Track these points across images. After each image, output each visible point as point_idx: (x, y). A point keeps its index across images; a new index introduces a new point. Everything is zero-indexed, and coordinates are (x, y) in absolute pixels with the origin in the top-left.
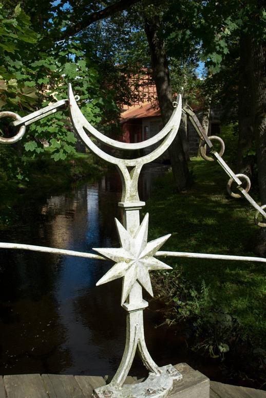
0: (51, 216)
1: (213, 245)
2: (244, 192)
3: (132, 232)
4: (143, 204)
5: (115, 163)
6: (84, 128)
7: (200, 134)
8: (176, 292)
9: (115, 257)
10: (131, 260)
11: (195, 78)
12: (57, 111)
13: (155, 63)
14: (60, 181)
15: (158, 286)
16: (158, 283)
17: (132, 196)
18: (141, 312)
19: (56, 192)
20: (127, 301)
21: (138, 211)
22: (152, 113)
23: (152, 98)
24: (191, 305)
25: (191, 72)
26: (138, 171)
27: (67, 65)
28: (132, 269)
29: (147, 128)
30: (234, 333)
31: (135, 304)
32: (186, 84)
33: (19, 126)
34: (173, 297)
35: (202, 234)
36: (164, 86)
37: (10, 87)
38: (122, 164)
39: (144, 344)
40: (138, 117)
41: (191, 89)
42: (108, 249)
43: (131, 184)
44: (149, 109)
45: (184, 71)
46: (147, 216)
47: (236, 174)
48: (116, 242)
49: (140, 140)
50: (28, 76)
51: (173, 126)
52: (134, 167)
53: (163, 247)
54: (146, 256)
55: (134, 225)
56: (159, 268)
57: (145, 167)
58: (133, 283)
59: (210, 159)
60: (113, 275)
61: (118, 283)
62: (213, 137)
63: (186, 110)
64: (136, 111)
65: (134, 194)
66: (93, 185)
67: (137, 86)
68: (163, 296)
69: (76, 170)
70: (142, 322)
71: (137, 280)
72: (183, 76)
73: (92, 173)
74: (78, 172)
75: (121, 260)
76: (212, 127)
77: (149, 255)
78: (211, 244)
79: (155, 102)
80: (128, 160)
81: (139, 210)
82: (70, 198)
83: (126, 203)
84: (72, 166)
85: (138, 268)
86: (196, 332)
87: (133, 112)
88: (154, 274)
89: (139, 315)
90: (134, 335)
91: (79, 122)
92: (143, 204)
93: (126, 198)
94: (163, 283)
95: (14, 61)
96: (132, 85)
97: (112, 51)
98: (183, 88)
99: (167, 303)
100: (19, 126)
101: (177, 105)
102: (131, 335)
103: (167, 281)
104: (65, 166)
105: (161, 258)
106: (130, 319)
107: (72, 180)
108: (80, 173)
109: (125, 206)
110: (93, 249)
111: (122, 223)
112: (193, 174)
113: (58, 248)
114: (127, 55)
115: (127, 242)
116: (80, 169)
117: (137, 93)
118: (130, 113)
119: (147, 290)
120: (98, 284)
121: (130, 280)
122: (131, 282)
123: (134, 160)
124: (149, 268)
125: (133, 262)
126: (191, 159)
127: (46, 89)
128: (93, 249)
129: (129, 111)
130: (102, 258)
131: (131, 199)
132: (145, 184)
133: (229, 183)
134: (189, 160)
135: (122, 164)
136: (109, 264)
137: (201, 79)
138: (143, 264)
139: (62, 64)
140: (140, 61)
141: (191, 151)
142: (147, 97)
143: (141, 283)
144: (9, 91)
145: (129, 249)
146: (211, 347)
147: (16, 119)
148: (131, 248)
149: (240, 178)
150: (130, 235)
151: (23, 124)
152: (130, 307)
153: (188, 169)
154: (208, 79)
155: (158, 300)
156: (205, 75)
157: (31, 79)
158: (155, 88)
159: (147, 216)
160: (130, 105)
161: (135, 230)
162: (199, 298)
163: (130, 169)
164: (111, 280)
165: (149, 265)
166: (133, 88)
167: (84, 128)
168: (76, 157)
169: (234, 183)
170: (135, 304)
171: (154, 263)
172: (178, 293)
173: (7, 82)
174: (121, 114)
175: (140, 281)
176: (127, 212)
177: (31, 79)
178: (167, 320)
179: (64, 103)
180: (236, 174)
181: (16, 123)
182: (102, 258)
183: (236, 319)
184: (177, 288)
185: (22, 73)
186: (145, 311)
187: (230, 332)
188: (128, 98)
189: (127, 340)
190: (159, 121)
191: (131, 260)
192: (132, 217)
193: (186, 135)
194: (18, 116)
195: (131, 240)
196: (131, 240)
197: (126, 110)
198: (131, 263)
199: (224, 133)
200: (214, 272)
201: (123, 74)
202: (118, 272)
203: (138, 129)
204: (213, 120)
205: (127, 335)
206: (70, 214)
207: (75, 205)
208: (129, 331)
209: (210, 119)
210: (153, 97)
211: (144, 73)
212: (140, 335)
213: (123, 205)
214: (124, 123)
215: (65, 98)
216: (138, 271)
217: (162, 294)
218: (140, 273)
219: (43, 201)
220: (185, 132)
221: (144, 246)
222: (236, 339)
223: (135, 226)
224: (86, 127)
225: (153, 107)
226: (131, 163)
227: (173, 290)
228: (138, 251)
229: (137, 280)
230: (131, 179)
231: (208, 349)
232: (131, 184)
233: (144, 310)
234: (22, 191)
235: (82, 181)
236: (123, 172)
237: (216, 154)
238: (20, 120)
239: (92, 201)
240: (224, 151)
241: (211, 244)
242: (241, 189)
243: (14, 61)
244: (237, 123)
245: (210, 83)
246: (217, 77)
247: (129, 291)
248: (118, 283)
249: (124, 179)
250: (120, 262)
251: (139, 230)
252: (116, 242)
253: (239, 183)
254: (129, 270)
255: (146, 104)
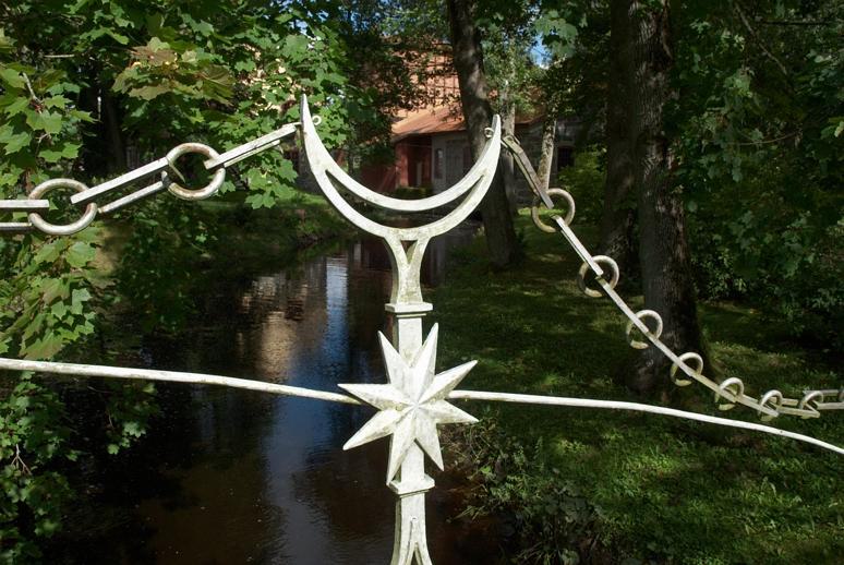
0: (260, 312)
1: (556, 371)
2: (607, 287)
3: (408, 356)
4: (429, 307)
5: (381, 235)
6: (327, 173)
7: (532, 186)
8: (486, 457)
9: (377, 401)
10: (406, 405)
11: (530, 64)
12: (281, 142)
13: (457, 36)
14: (277, 246)
15: (454, 444)
16: (454, 440)
17: (410, 294)
18: (422, 497)
19: (270, 267)
20: (398, 477)
21: (420, 320)
22: (452, 123)
23: (451, 99)
24: (515, 483)
25: (522, 53)
26: (421, 249)
27: (291, 39)
28: (408, 420)
29: (440, 152)
30: (589, 532)
31: (411, 482)
32: (513, 75)
33: (214, 170)
34: (480, 466)
35: (536, 351)
36: (474, 78)
37: (185, 65)
38: (392, 236)
39: (425, 552)
40: (423, 131)
41: (523, 86)
42: (366, 386)
43: (408, 272)
44: (445, 119)
45: (510, 51)
46: (436, 328)
47: (593, 255)
48: (380, 375)
49: (430, 193)
50: (217, 56)
51: (484, 171)
52: (414, 242)
53: (464, 384)
54: (432, 398)
55: (413, 344)
56: (455, 421)
57: (433, 241)
58: (408, 445)
59: (550, 229)
60: (373, 432)
61: (382, 446)
62: (554, 191)
63: (509, 143)
64: (420, 120)
65: (414, 289)
66: (337, 255)
67: (423, 76)
68: (463, 464)
69: (306, 228)
70: (422, 513)
71: (416, 441)
72: (509, 60)
73: (336, 234)
74: (309, 232)
75: (389, 404)
76: (559, 156)
77: (437, 397)
78: (553, 370)
79: (456, 104)
80: (404, 230)
81: (422, 317)
82: (295, 278)
83: (399, 304)
84: (299, 219)
85: (418, 421)
86: (521, 530)
87: (415, 122)
88: (449, 432)
89: (418, 501)
90: (408, 536)
91: (318, 162)
92: (429, 307)
93: (399, 296)
94: (463, 439)
95: (198, 22)
96: (413, 74)
97: (379, 11)
98: (507, 83)
99: (471, 478)
100: (214, 170)
101: (492, 134)
102: (403, 540)
103: (470, 437)
104: (286, 220)
105: (457, 402)
106: (403, 509)
107: (300, 245)
108: (314, 232)
109: (396, 311)
110: (340, 385)
111: (391, 343)
112: (524, 240)
113: (271, 381)
114: (406, 18)
115: (399, 373)
116: (314, 225)
117: (421, 87)
118: (409, 124)
119: (433, 459)
120: (346, 447)
121: (403, 441)
122: (404, 444)
123: (414, 229)
124: (438, 421)
125: (409, 409)
126: (520, 211)
127: (256, 76)
128: (340, 385)
129: (407, 121)
130: (355, 401)
131: (408, 297)
132: (435, 264)
133: (583, 270)
134: (516, 214)
135: (392, 236)
136: (367, 411)
137: (542, 66)
138: (427, 412)
139: (281, 37)
140: (430, 31)
141: (521, 198)
142: (441, 95)
143: (423, 445)
144: (182, 73)
145: (403, 386)
146: (548, 557)
147: (207, 157)
148: (407, 385)
149: (601, 264)
150: (404, 363)
151: (221, 166)
152: (401, 488)
153: (513, 230)
154: (553, 67)
155: (454, 471)
156: (549, 59)
157: (222, 62)
158: (457, 80)
159: (436, 328)
160: (409, 108)
161: (414, 353)
162: (528, 469)
163: (408, 245)
164: (370, 440)
165: (437, 415)
166: (414, 79)
167: (327, 173)
168: (307, 203)
169: (590, 272)
170: (411, 482)
171: (445, 411)
172: (490, 458)
173: (179, 56)
174: (393, 126)
175: (421, 443)
176: (400, 321)
177: (222, 62)
178: (469, 507)
179: (293, 130)
180: (593, 255)
181: (209, 165)
182: (355, 401)
183: (593, 508)
184: (490, 449)
185: (208, 50)
186: (430, 496)
187: (582, 529)
188: (409, 98)
189: (396, 545)
190: (464, 141)
191: (407, 405)
192: (409, 329)
193: (506, 172)
194: (212, 152)
195: (407, 370)
196: (407, 370)
197: (401, 119)
198: (406, 410)
199: (581, 167)
200: (557, 421)
201: (397, 54)
202: (381, 427)
203: (426, 163)
204: (562, 141)
205: (397, 536)
206: (294, 313)
207: (304, 292)
208: (400, 530)
209: (557, 139)
210: (451, 95)
211: (437, 53)
212: (419, 537)
213: (393, 309)
214: (397, 142)
215: (296, 120)
216: (418, 425)
217: (461, 460)
218: (421, 429)
219: (246, 283)
220: (509, 167)
221: (428, 382)
222: (592, 542)
223: (413, 345)
224: (331, 171)
225: (453, 115)
226: (409, 234)
227: (482, 453)
228: (419, 392)
229: (416, 441)
230: (409, 262)
231: (543, 559)
232: (408, 272)
233: (426, 494)
234: (206, 264)
235: (318, 248)
236: (394, 251)
237: (560, 221)
238: (216, 158)
239: (337, 281)
240: (574, 211)
241: (553, 370)
242: (602, 282)
243: (198, 22)
244: (605, 150)
245: (551, 81)
246: (569, 66)
247: (402, 459)
248: (382, 446)
249: (396, 264)
250: (386, 408)
251: (419, 353)
252: (380, 375)
253: (599, 271)
254: (402, 424)
255: (441, 109)
